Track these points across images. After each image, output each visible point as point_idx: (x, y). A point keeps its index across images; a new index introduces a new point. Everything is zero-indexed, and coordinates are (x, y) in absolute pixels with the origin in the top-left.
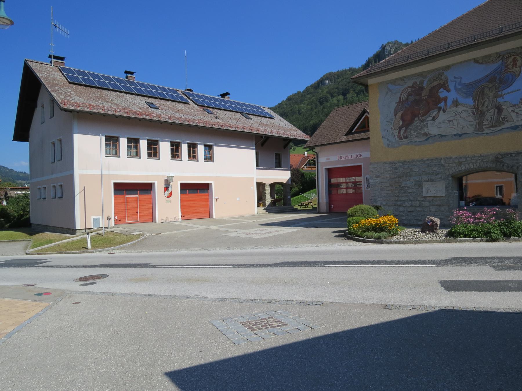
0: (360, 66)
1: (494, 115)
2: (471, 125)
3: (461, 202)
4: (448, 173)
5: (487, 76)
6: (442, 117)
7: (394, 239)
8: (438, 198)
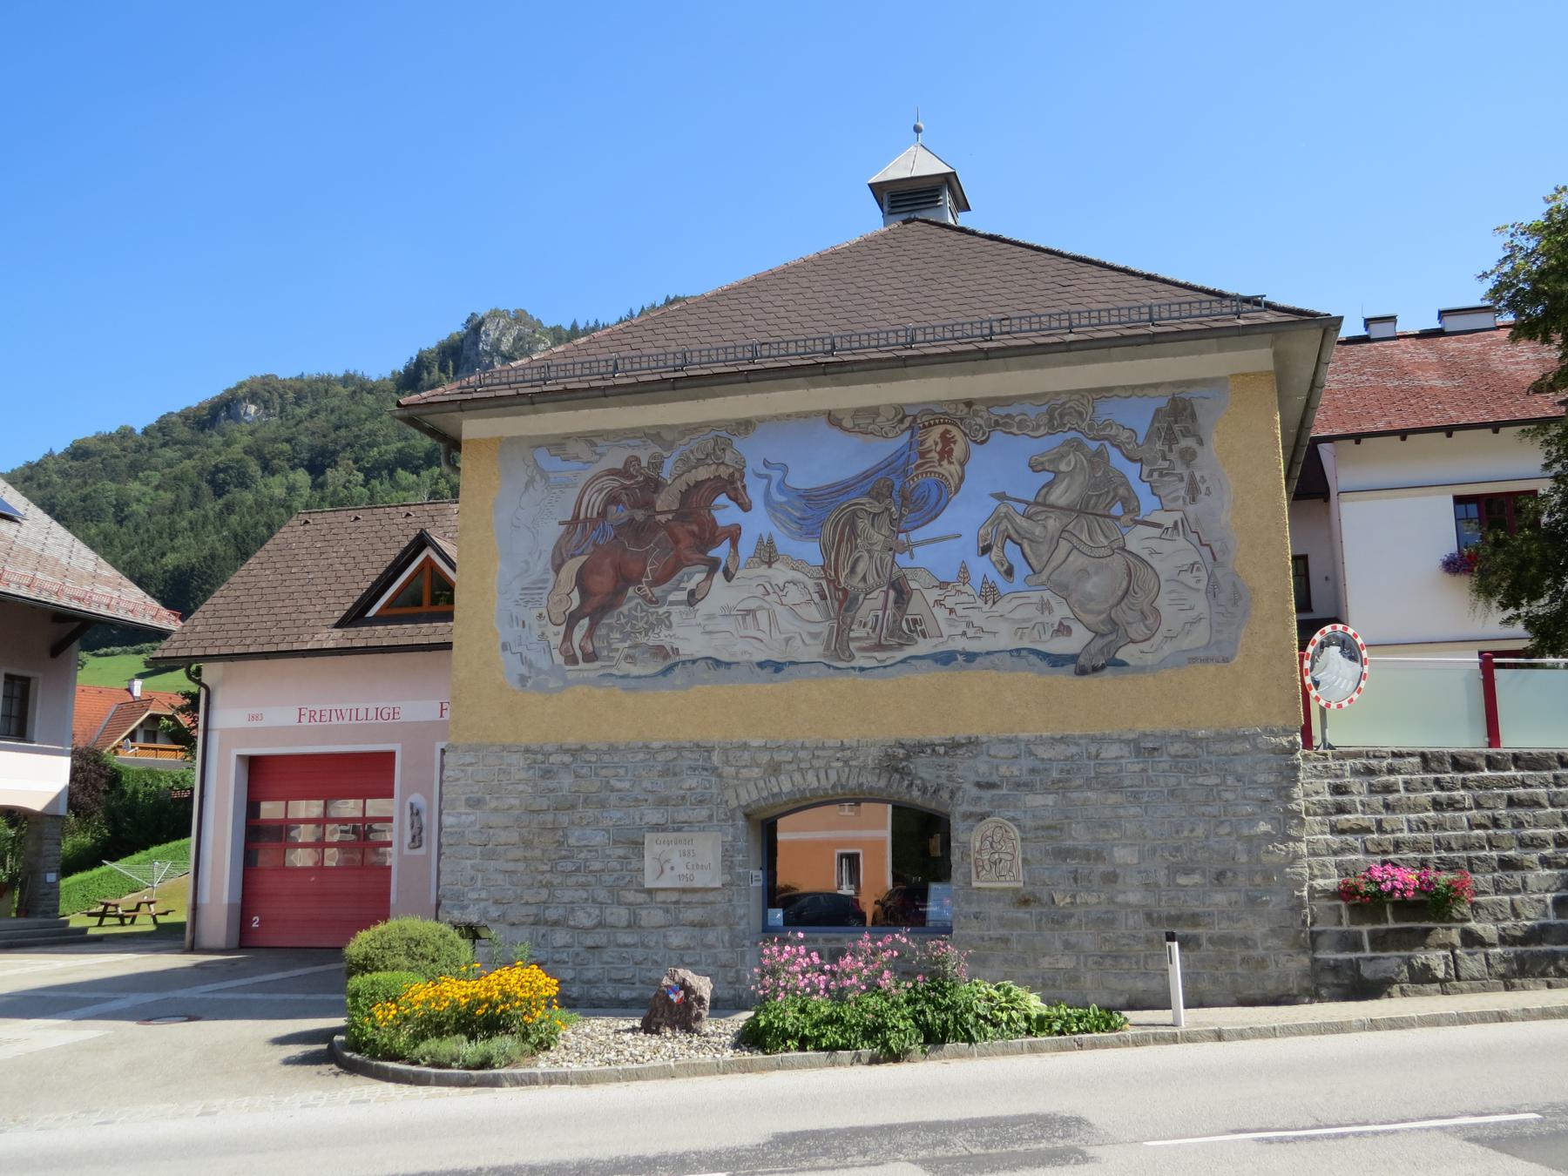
0: (388, 375)
1: (885, 608)
2: (815, 636)
3: (771, 911)
4: (733, 803)
5: (866, 476)
6: (720, 594)
7: (542, 1065)
8: (697, 897)
